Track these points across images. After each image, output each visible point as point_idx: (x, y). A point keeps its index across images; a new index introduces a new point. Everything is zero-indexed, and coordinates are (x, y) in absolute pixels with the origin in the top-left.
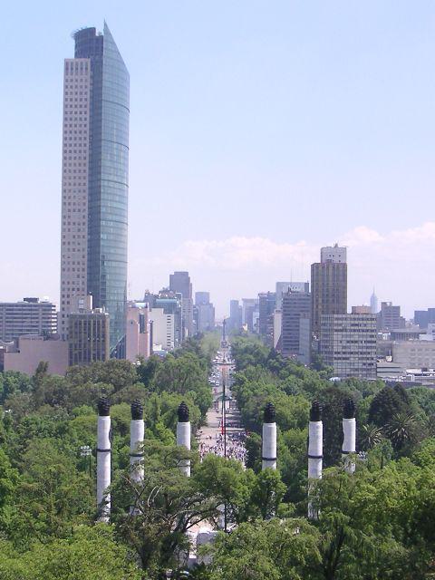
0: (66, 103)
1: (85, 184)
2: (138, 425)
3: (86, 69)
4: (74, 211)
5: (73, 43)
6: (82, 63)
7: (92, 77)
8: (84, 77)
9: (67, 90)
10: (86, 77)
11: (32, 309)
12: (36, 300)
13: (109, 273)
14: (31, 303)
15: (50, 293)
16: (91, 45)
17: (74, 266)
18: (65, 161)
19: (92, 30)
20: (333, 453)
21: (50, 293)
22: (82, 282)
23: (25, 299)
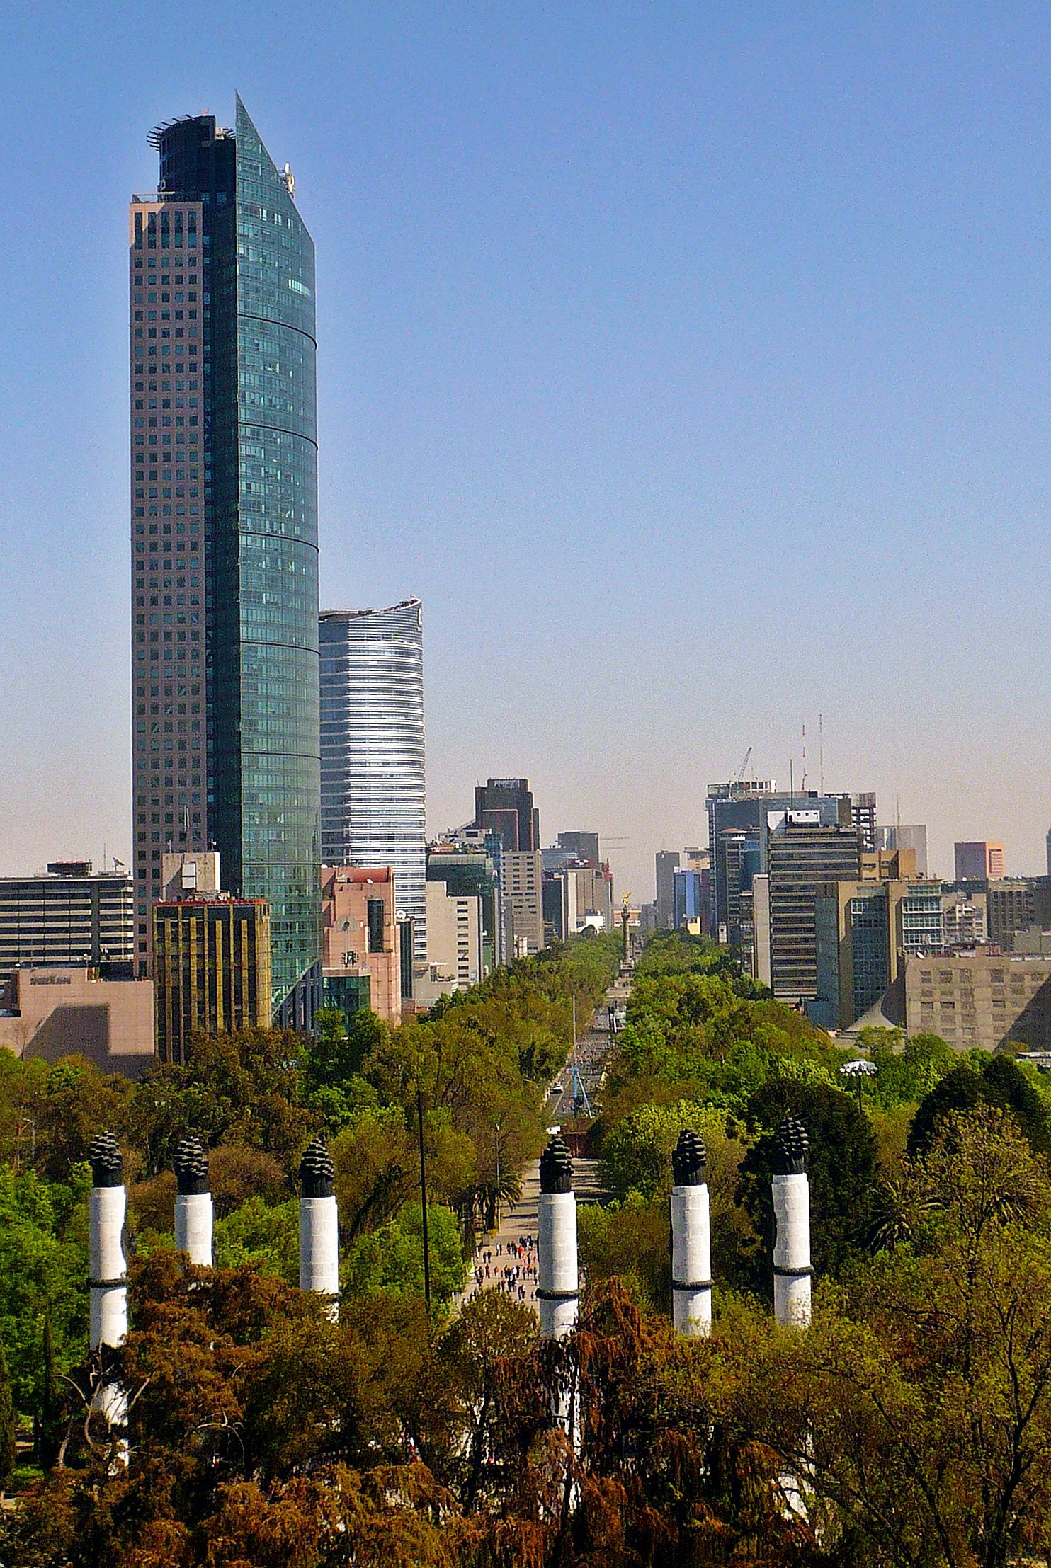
0: (139, 378)
1: (193, 261)
2: (308, 1216)
3: (192, 229)
4: (166, 334)
5: (153, 159)
6: (179, 214)
7: (207, 252)
8: (186, 252)
9: (139, 378)
10: (192, 247)
11: (71, 879)
12: (81, 868)
13: (247, 623)
14: (70, 878)
15: (110, 849)
16: (199, 162)
17: (179, 324)
18: (138, 467)
19: (202, 126)
20: (748, 1266)
21: (110, 849)
22: (191, 802)
23: (52, 867)
